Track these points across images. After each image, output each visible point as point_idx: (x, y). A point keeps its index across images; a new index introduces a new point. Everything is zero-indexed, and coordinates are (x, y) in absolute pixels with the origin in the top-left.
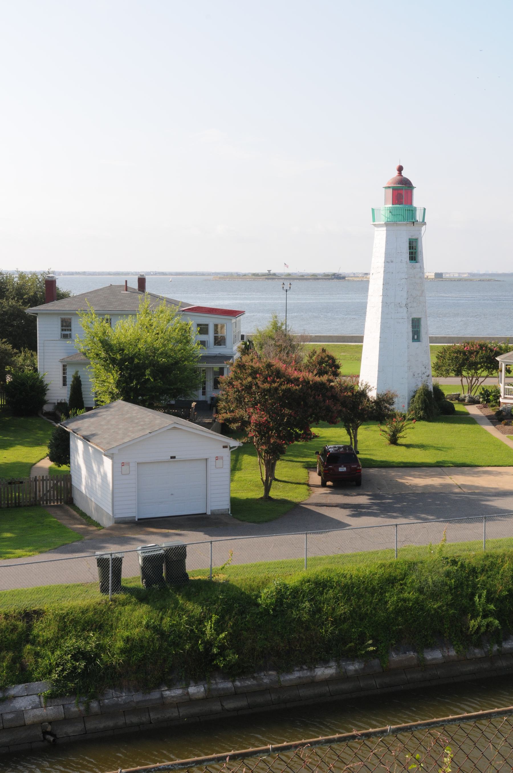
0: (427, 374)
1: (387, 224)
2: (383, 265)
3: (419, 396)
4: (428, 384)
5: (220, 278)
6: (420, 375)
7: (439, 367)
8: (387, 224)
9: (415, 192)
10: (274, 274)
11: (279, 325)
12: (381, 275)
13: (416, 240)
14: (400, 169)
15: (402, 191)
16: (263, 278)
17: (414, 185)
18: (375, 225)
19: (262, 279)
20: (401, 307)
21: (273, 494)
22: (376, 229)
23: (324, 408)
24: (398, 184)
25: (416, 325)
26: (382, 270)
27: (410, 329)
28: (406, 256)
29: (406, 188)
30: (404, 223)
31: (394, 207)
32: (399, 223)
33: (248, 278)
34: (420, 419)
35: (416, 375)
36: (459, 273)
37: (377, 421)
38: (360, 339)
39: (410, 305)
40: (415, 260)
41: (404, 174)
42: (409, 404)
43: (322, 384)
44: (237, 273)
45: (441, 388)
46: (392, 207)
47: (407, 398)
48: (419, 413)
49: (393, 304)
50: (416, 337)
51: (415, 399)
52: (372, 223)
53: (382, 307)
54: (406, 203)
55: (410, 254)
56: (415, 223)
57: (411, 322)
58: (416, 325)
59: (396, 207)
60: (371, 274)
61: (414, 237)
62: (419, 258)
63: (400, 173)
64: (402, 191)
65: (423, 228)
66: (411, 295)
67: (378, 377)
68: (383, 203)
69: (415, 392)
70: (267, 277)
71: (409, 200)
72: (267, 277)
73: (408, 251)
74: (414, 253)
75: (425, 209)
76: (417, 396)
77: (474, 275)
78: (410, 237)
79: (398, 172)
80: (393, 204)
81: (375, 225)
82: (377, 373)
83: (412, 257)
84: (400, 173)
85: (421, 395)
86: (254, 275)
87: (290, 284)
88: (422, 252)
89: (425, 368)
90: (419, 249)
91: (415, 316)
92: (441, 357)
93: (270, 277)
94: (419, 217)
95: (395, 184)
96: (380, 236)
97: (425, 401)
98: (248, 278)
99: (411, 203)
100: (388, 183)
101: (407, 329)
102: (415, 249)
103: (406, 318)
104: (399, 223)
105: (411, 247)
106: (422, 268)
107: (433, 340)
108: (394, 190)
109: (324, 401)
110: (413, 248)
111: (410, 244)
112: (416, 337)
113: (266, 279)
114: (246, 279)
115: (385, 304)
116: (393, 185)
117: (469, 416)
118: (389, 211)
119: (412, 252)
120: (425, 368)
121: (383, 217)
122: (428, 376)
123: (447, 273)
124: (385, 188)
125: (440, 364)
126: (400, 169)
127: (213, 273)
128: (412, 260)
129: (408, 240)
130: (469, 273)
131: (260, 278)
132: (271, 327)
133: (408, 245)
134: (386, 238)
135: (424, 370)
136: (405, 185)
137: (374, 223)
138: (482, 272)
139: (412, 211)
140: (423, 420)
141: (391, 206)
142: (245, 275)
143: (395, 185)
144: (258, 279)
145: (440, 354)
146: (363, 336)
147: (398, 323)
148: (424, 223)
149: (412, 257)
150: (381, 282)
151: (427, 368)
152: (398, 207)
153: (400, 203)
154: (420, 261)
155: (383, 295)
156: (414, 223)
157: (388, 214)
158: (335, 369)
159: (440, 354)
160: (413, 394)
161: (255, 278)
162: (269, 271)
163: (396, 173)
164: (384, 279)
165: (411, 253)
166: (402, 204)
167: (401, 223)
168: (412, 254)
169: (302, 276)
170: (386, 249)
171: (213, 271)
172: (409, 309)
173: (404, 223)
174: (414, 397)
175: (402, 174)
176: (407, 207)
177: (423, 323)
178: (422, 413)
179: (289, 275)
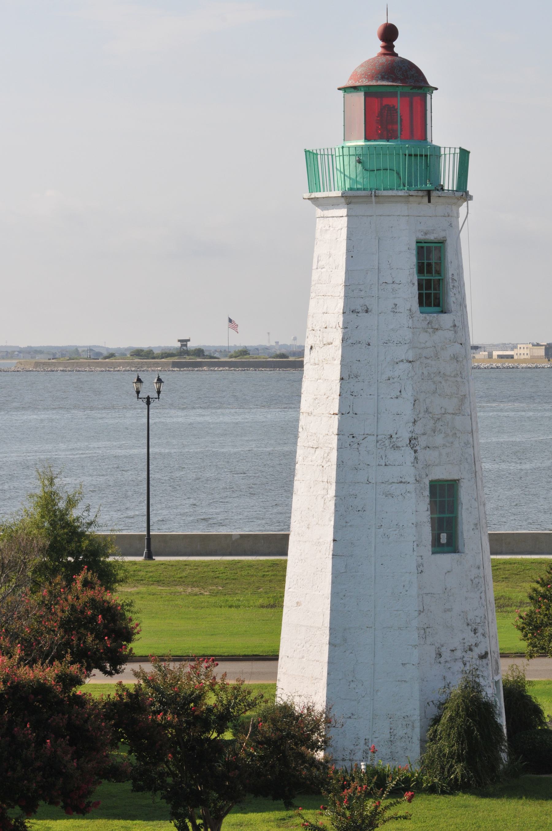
0: (478, 651)
1: (349, 199)
2: (341, 319)
3: (451, 719)
4: (481, 681)
5: (37, 364)
6: (459, 654)
7: (537, 628)
8: (349, 199)
10: (199, 352)
11: (62, 505)
12: (336, 352)
13: (441, 244)
14: (389, 34)
15: (395, 96)
16: (166, 364)
17: (431, 82)
18: (314, 200)
19: (163, 365)
20: (396, 447)
22: (319, 212)
23: (38, 764)
24: (383, 78)
25: (444, 498)
26: (337, 336)
28: (409, 294)
29: (407, 90)
30: (401, 193)
31: (369, 147)
32: (385, 193)
33: (120, 364)
34: (453, 788)
35: (446, 655)
37: (275, 798)
38: (279, 544)
39: (423, 441)
40: (437, 305)
41: (401, 48)
42: (423, 741)
43: (41, 689)
44: (90, 350)
45: (530, 691)
46: (362, 147)
47: (417, 724)
48: (450, 771)
49: (374, 438)
50: (444, 538)
51: (440, 728)
52: (307, 195)
53: (340, 448)
54: (411, 136)
56: (434, 194)
57: (427, 493)
58: (444, 498)
59: (375, 147)
60: (307, 351)
61: (431, 237)
62: (452, 299)
63: (389, 47)
64: (395, 96)
66: (427, 411)
67: (330, 663)
69: (441, 706)
70: (176, 359)
71: (417, 124)
72: (176, 359)
73: (415, 279)
74: (434, 281)
76: (444, 720)
77: (31, 347)
78: (421, 237)
79: (381, 43)
80: (367, 138)
81: (314, 200)
82: (326, 648)
83: (428, 296)
84: (389, 47)
85: (457, 714)
86: (138, 353)
87: (159, 381)
89: (475, 631)
90: (451, 270)
91: (441, 473)
92: (544, 597)
93: (187, 359)
95: (372, 78)
96: (332, 231)
97: (468, 732)
98: (120, 364)
100: (354, 76)
101: (416, 511)
102: (438, 273)
103: (412, 480)
104: (385, 193)
105: (423, 267)
106: (460, 328)
107: (500, 543)
108: (370, 94)
109: (40, 742)
112: (444, 538)
113: (175, 365)
114: (113, 365)
115: (348, 439)
116: (366, 82)
118: (353, 159)
119: (428, 282)
120: (475, 631)
121: (342, 172)
122: (484, 656)
125: (539, 618)
126: (389, 34)
127: (21, 351)
128: (429, 305)
129: (414, 246)
131: (157, 365)
132: (37, 513)
133: (413, 260)
134: (349, 239)
135: (471, 639)
136: (402, 81)
137: (314, 195)
139: (430, 158)
140: (464, 792)
141: (361, 143)
142: (111, 356)
143: (374, 83)
144: (149, 365)
145: (541, 590)
146: (287, 537)
147: (388, 495)
148: (462, 193)
149: (428, 296)
150: (334, 372)
151: (480, 631)
152: (382, 147)
153: (389, 136)
155: (341, 413)
156: (429, 193)
157: (351, 168)
158: (115, 641)
159: (541, 590)
160: (433, 711)
161: (142, 365)
162: (184, 342)
163: (377, 46)
164: (344, 364)
166: (396, 138)
167: (390, 193)
168: (428, 287)
169: (283, 356)
170: (349, 272)
171: (23, 344)
172: (420, 455)
173: (401, 193)
174: (436, 720)
175: (396, 50)
176: (408, 146)
177: (465, 495)
178: (458, 769)
179: (244, 352)
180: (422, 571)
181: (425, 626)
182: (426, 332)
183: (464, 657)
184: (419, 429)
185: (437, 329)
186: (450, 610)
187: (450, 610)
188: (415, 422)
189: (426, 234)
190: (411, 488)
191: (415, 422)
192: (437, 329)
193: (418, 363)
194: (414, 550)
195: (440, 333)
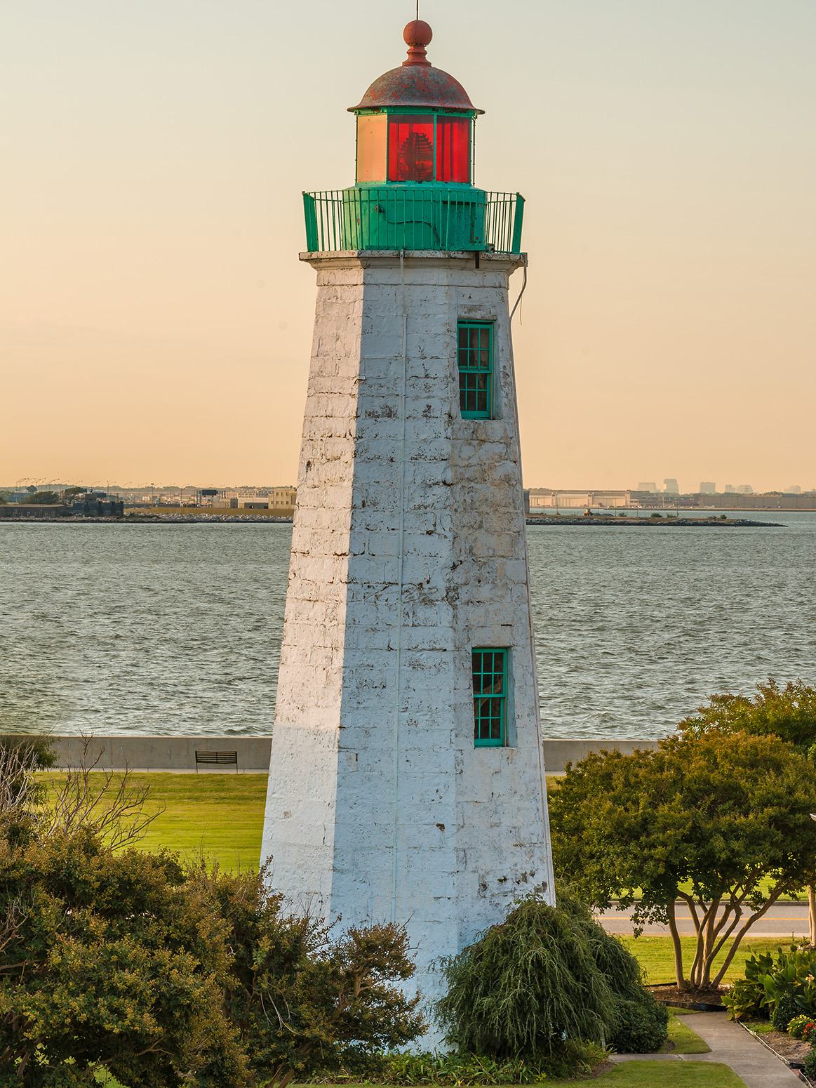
9: (480, 128)
14: (419, 35)
15: (424, 119)
20: (428, 602)
21: (346, 550)
27: (466, 695)
30: (439, 254)
32: (417, 254)
36: (595, 494)
39: (464, 594)
40: (483, 407)
41: (436, 55)
55: (462, 384)
57: (469, 664)
61: (478, 315)
64: (424, 119)
65: (516, 278)
68: (339, 156)
74: (479, 372)
75: (520, 200)
88: (509, 375)
94: (497, 235)
99: (466, 177)
101: (451, 689)
102: (486, 364)
103: (450, 646)
104: (417, 254)
110: (473, 362)
111: (462, 342)
117: (710, 1058)
123: (544, 492)
124: (358, 110)
126: (419, 35)
129: (455, 326)
130: (634, 494)
138: (686, 488)
147: (416, 666)
148: (517, 260)
149: (471, 395)
154: (505, 411)
165: (466, 380)
168: (471, 384)
175: (428, 58)
177: (517, 666)
180: (462, 771)
181: (466, 847)
182: (470, 444)
183: (515, 889)
184: (459, 577)
185: (484, 441)
186: (497, 825)
187: (497, 825)
188: (454, 567)
189: (470, 310)
190: (447, 657)
191: (454, 567)
192: (484, 441)
193: (459, 486)
194: (451, 742)
195: (486, 446)
